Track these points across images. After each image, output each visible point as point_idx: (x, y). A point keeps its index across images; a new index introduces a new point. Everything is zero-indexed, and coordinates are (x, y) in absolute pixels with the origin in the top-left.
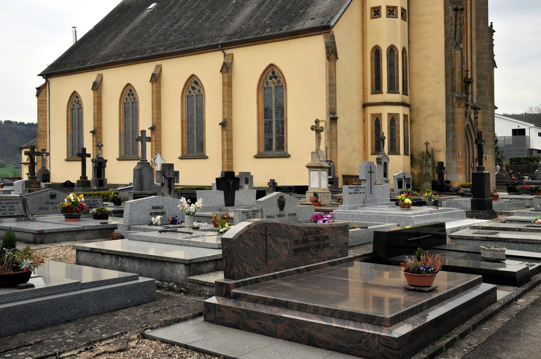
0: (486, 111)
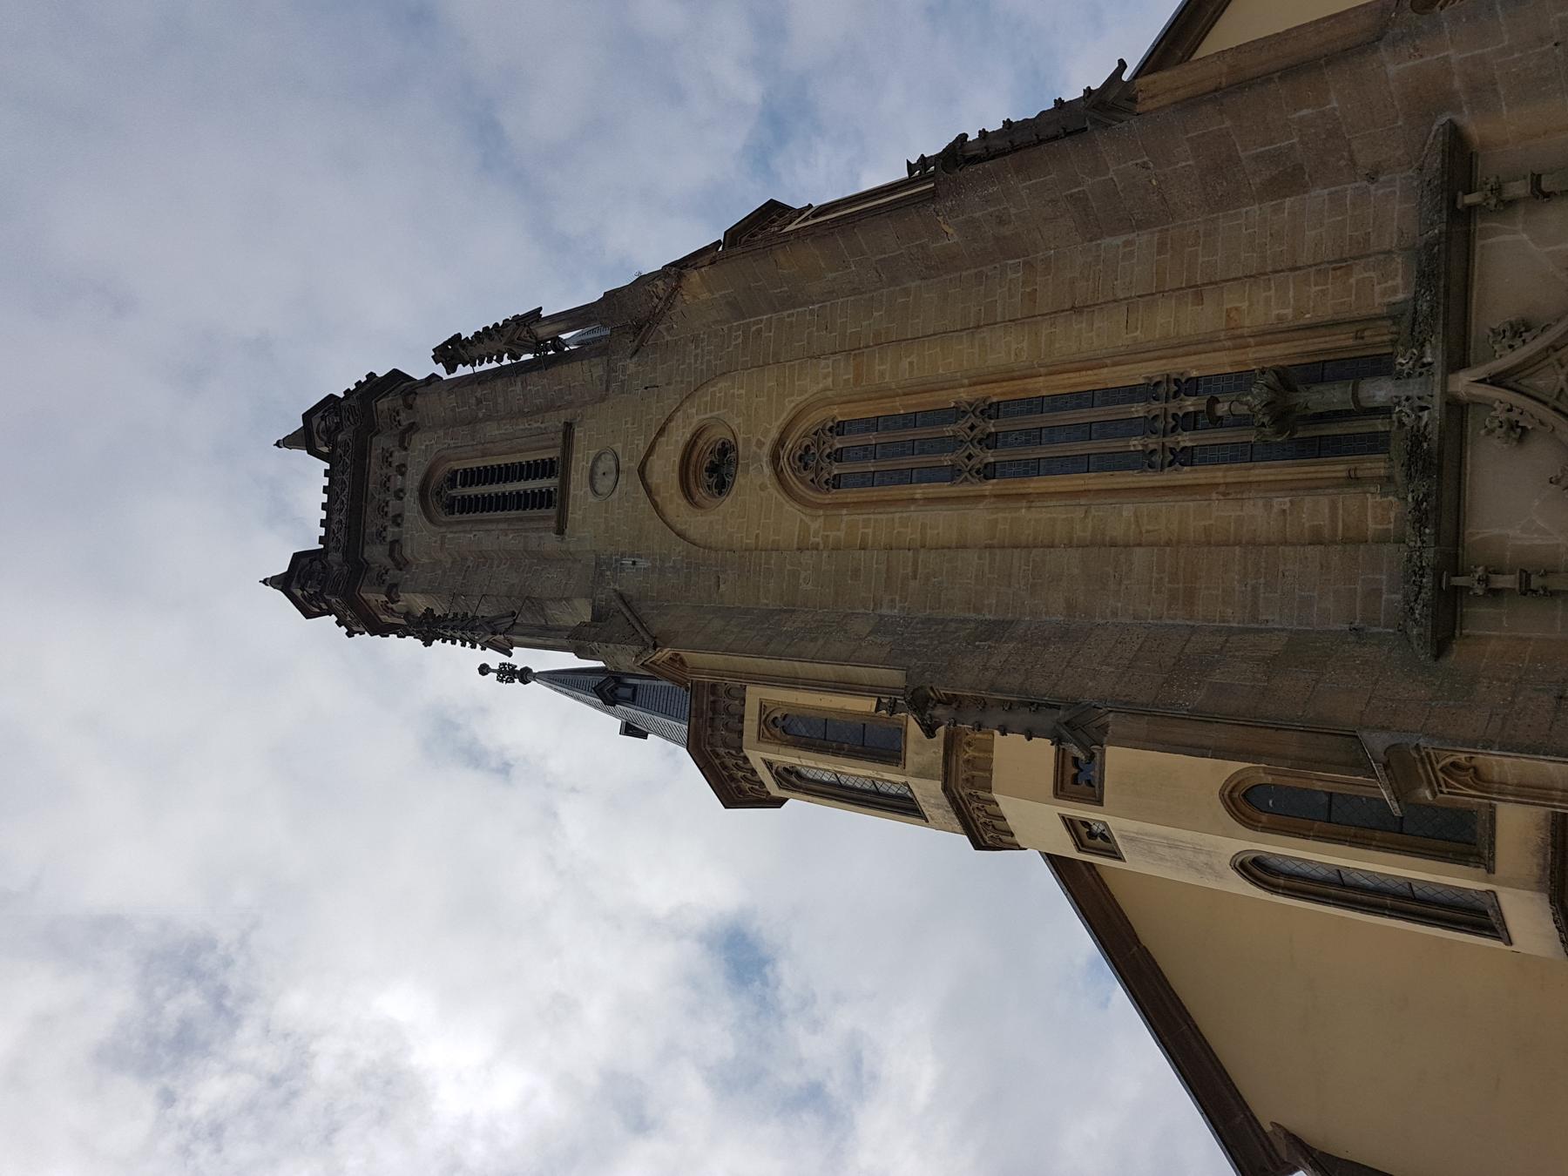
0: (1457, 84)
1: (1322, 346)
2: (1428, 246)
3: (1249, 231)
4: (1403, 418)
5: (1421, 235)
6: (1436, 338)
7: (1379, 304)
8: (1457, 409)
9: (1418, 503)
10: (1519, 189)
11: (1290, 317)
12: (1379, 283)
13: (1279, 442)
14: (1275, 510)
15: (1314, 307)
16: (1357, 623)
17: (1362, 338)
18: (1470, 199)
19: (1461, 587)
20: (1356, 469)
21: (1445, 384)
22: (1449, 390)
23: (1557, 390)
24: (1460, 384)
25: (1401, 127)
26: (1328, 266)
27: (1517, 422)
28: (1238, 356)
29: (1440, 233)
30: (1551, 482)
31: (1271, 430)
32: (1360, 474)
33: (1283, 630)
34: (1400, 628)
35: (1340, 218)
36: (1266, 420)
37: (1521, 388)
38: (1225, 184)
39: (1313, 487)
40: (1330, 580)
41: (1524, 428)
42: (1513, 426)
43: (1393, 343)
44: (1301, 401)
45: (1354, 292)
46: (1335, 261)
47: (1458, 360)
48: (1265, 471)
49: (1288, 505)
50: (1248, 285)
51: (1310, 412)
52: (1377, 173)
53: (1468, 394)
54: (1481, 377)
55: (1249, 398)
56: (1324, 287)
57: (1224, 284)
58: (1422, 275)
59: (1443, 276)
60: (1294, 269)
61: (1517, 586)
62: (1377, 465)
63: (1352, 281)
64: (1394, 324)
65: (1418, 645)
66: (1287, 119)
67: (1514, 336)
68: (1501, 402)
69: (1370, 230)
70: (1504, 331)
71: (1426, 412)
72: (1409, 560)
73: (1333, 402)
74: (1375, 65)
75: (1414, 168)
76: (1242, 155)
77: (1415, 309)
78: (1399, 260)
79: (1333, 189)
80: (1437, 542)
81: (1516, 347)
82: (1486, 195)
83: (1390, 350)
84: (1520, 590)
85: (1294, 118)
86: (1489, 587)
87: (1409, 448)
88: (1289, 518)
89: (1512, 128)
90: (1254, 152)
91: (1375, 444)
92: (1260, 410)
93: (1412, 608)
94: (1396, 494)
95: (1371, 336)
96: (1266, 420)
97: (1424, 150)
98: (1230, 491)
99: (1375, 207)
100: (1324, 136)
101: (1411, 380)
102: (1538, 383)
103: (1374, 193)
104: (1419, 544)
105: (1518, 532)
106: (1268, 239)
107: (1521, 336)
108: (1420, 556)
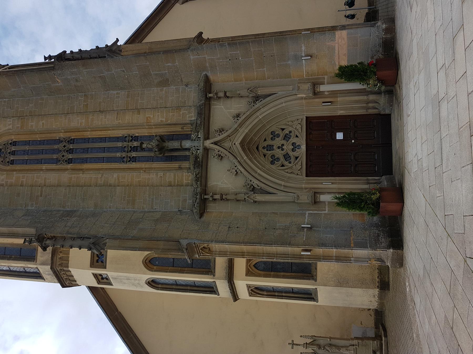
1: (173, 130)
8: (206, 150)
9: (196, 175)
10: (221, 94)
12: (188, 114)
14: (159, 176)
15: (171, 119)
16: (180, 209)
18: (210, 95)
19: (207, 198)
20: (181, 165)
21: (203, 143)
22: (204, 145)
25: (194, 73)
26: (175, 108)
27: (220, 154)
32: (182, 166)
36: (157, 150)
38: (147, 80)
39: (170, 170)
41: (222, 156)
42: (220, 156)
45: (181, 116)
46: (177, 107)
47: (207, 137)
49: (163, 175)
52: (188, 84)
54: (212, 142)
55: (152, 143)
56: (174, 114)
58: (198, 113)
63: (181, 113)
65: (196, 214)
70: (218, 130)
71: (199, 150)
77: (197, 122)
80: (201, 186)
86: (214, 198)
88: (162, 178)
91: (186, 158)
93: (194, 204)
96: (157, 150)
100: (174, 72)
101: (195, 142)
104: (196, 186)
107: (221, 132)
108: (197, 190)
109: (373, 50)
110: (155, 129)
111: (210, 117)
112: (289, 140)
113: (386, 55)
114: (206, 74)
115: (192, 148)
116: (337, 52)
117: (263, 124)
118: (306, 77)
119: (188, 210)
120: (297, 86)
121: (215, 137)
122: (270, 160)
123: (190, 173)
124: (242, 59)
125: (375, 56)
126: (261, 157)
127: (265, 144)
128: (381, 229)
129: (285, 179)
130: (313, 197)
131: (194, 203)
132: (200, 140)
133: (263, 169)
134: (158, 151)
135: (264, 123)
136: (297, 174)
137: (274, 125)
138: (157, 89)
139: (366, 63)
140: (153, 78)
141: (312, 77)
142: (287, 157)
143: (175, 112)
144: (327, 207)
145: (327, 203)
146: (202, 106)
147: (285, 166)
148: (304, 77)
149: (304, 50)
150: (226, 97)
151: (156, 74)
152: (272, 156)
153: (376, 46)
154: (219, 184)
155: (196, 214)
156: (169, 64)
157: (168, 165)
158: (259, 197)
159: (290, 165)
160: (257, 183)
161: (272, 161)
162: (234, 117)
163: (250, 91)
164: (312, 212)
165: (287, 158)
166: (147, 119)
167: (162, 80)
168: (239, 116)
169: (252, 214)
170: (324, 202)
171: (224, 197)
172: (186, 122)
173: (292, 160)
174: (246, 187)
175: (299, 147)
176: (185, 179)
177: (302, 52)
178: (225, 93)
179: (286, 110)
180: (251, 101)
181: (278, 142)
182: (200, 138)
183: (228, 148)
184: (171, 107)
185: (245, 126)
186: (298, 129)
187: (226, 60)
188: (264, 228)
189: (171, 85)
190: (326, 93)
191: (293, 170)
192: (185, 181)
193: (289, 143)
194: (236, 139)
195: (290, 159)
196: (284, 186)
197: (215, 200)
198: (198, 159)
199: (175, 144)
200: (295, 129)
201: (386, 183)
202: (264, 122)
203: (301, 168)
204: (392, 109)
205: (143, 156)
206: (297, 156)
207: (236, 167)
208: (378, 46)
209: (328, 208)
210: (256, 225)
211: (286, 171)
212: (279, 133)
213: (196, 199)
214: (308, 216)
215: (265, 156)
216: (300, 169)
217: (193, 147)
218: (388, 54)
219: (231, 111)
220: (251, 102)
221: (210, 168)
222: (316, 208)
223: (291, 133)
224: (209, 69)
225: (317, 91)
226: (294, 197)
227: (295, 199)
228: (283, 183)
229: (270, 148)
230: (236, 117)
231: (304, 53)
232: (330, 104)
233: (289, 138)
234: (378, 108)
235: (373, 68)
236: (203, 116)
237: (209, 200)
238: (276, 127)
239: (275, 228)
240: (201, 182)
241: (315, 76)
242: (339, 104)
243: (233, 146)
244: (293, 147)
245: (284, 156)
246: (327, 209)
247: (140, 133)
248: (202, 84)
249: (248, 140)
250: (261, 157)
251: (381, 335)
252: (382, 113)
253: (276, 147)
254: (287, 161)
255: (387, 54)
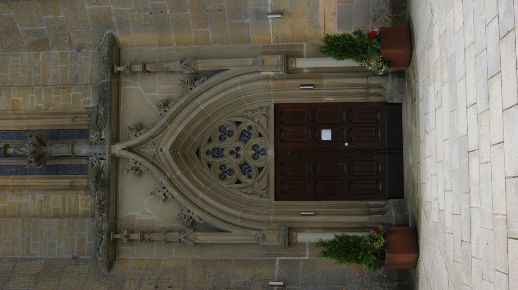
1: (58, 123)
2: (103, 86)
3: (23, 64)
4: (93, 163)
5: (100, 80)
6: (107, 129)
7: (82, 107)
8: (115, 160)
9: (100, 201)
10: (138, 68)
11: (43, 108)
12: (82, 98)
13: (38, 169)
14: (37, 200)
15: (54, 104)
16: (75, 254)
17: (75, 121)
18: (120, 69)
19: (118, 239)
20: (73, 182)
21: (110, 149)
22: (112, 152)
23: (153, 155)
24: (116, 150)
25: (91, 31)
26: (60, 86)
27: (138, 168)
28: (19, 123)
29: (108, 82)
30: (151, 194)
31: (35, 164)
32: (75, 184)
33: (41, 259)
34: (94, 256)
35: (65, 66)
36: (32, 160)
37: (139, 153)
38: (11, 40)
39: (55, 190)
40: (63, 235)
41: (141, 170)
42: (137, 169)
43: (89, 125)
44: (49, 151)
45: (71, 100)
46: (63, 85)
47: (115, 139)
48: (32, 181)
49: (43, 198)
50: (22, 90)
51: (52, 156)
52: (81, 48)
53: (120, 154)
54: (125, 147)
55: (24, 149)
56: (58, 96)
57: (11, 87)
58: (100, 98)
59: (109, 101)
60: (44, 85)
61: (139, 239)
62: (82, 180)
63: (71, 95)
64: (89, 117)
65: (101, 265)
66: (41, 18)
67: (137, 131)
68: (132, 159)
69: (78, 74)
70: (133, 129)
71: (103, 161)
72: (97, 226)
73: (63, 153)
74: (80, 4)
75: (96, 49)
76: (20, 29)
77: (98, 113)
78: (91, 89)
79: (62, 51)
80: (108, 219)
81: (137, 136)
82: (125, 69)
83: (87, 128)
84: (141, 240)
85: (44, 18)
86: (129, 239)
87: (96, 175)
88: (43, 204)
89: (135, 41)
90: (25, 29)
91: (81, 170)
92: (29, 155)
93: (98, 248)
94: (91, 195)
95: (79, 121)
96: (32, 160)
97: (100, 43)
98: (15, 190)
99: (80, 63)
100: (58, 28)
101: (96, 146)
102: (146, 151)
103: (80, 57)
104: (101, 220)
105: (139, 214)
106: (32, 70)
107: (139, 131)
108: (101, 225)
109: (375, 9)
110: (28, 121)
111: (120, 105)
112: (247, 141)
113: (394, 17)
114: (111, 33)
115: (91, 156)
116: (321, 9)
117: (206, 117)
118: (273, 43)
119: (88, 256)
120: (260, 60)
121: (128, 138)
122: (219, 172)
123: (90, 195)
124: (172, 13)
125: (379, 17)
126: (204, 167)
127: (211, 146)
128: (386, 285)
129: (243, 206)
130: (287, 237)
131: (98, 246)
132: (105, 144)
133: (207, 190)
134: (35, 162)
135: (209, 115)
136: (261, 196)
137: (223, 116)
138: (29, 54)
139: (365, 33)
140: (22, 37)
141: (283, 44)
142: (244, 168)
143: (61, 93)
144: (307, 250)
145: (307, 245)
146: (107, 87)
147: (242, 183)
148: (271, 43)
149: (271, 4)
150: (145, 71)
151: (27, 32)
152: (221, 166)
153: (381, 4)
154: (138, 214)
155: (103, 264)
156: (49, 16)
157: (51, 181)
158: (202, 237)
159: (250, 181)
160: (199, 214)
161: (221, 174)
162: (159, 107)
163: (185, 64)
164: (284, 258)
165: (245, 170)
166: (13, 103)
167: (36, 40)
168: (167, 105)
169: (192, 263)
170: (304, 244)
171: (146, 236)
172: (79, 110)
173: (254, 173)
174: (181, 220)
175: (264, 153)
176: (82, 205)
177: (268, 6)
178: (144, 65)
179: (243, 94)
180: (186, 81)
181: (231, 143)
182: (104, 139)
183: (150, 157)
184: (54, 85)
185: (177, 120)
186: (262, 124)
187: (145, 14)
188: (212, 288)
189: (52, 48)
190: (306, 71)
191: (254, 189)
192: (82, 209)
193: (248, 146)
194: (164, 141)
195: (250, 171)
196: (241, 218)
197: (131, 240)
198: (102, 176)
199: (63, 149)
200: (257, 123)
201: (394, 215)
202: (207, 114)
203: (268, 186)
204: (403, 97)
205: (9, 165)
206: (261, 166)
207: (164, 188)
208: (383, 3)
209: (309, 251)
210: (199, 282)
211: (244, 190)
212: (231, 129)
213: (102, 239)
214: (278, 265)
215: (210, 165)
216: (266, 187)
217: (93, 156)
218: (397, 17)
219: (154, 94)
220: (187, 82)
221: (121, 188)
222: (290, 253)
223: (250, 128)
224: (117, 25)
225: (292, 68)
226: (257, 237)
227: (259, 240)
228: (240, 214)
229: (218, 153)
230: (162, 107)
231: (271, 9)
232: (311, 87)
233: (247, 136)
234: (383, 95)
235: (375, 43)
236: (108, 104)
237: (122, 242)
238: (228, 119)
239: (228, 287)
240: (108, 212)
241: (288, 42)
242: (325, 88)
243: (159, 153)
244: (254, 152)
245: (241, 166)
246: (307, 253)
247: (2, 126)
248: (105, 50)
249: (184, 141)
250: (204, 167)
251: (405, 224)
252: (389, 101)
253: (227, 152)
254: (245, 174)
255: (397, 16)
